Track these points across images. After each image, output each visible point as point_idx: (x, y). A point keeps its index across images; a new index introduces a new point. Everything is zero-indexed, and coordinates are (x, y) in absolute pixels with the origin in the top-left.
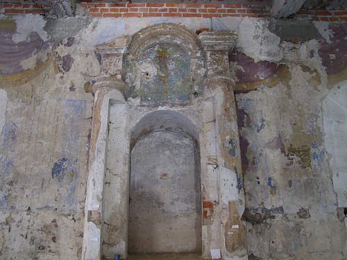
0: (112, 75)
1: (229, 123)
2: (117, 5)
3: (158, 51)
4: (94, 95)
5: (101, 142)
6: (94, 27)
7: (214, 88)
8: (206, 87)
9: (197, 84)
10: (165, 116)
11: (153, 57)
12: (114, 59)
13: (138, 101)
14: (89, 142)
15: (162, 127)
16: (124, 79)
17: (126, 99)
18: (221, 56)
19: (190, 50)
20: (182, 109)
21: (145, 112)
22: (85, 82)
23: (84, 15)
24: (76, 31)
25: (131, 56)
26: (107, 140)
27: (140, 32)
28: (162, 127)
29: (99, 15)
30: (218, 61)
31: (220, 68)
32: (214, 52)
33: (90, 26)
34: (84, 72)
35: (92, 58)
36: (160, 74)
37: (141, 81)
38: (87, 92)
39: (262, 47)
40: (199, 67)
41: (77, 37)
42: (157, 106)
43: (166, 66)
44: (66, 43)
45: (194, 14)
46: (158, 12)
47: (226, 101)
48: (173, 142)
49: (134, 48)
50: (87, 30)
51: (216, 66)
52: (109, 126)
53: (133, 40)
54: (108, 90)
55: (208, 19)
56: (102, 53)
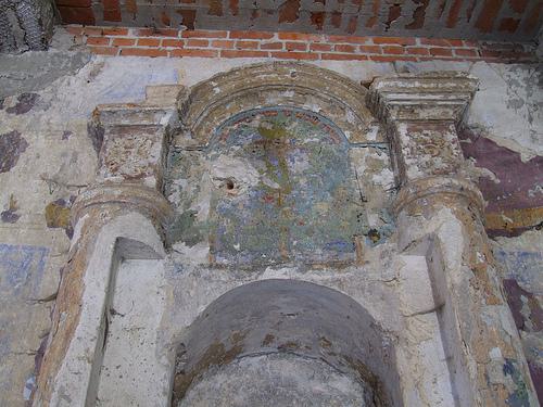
0: (129, 178)
1: (491, 310)
2: (157, 33)
3: (261, 130)
4: (70, 234)
5: (76, 366)
6: (93, 75)
7: (429, 212)
8: (403, 212)
9: (374, 210)
10: (281, 300)
11: (247, 141)
12: (139, 138)
13: (201, 253)
14: (37, 371)
15: (269, 339)
16: (162, 188)
17: (167, 246)
18: (438, 134)
19: (349, 126)
20: (337, 275)
21: (222, 284)
22: (51, 199)
23: (71, 50)
24: (42, 83)
25: (185, 140)
26: (97, 363)
27: (213, 79)
28: (269, 339)
29: (110, 52)
30: (430, 146)
31: (439, 163)
32: (416, 125)
33: (83, 72)
34: (52, 172)
35: (81, 143)
36: (268, 182)
37: (214, 202)
38: (52, 225)
39: (534, 126)
40: (375, 167)
41: (44, 94)
42: (258, 267)
43: (283, 165)
44: (12, 105)
45: (348, 55)
46: (259, 49)
47: (472, 244)
48: (302, 386)
49: (195, 118)
50: (73, 79)
51: (427, 158)
52: (106, 323)
53: (191, 100)
54: (116, 214)
55: (387, 64)
56: (107, 123)
